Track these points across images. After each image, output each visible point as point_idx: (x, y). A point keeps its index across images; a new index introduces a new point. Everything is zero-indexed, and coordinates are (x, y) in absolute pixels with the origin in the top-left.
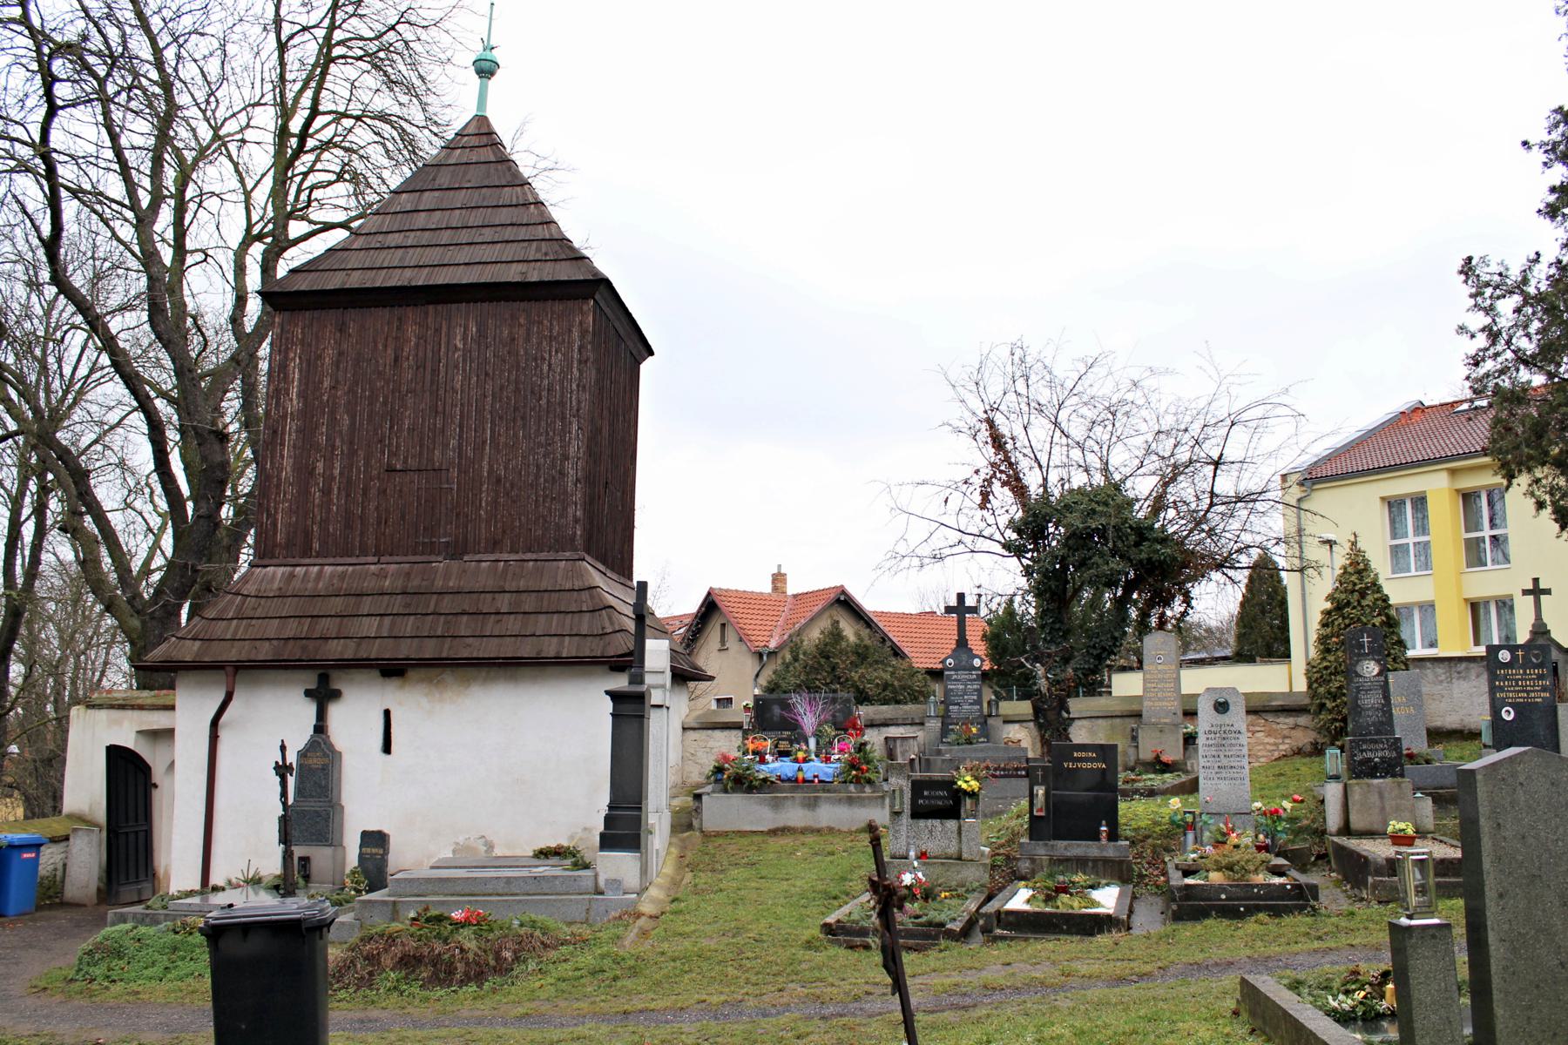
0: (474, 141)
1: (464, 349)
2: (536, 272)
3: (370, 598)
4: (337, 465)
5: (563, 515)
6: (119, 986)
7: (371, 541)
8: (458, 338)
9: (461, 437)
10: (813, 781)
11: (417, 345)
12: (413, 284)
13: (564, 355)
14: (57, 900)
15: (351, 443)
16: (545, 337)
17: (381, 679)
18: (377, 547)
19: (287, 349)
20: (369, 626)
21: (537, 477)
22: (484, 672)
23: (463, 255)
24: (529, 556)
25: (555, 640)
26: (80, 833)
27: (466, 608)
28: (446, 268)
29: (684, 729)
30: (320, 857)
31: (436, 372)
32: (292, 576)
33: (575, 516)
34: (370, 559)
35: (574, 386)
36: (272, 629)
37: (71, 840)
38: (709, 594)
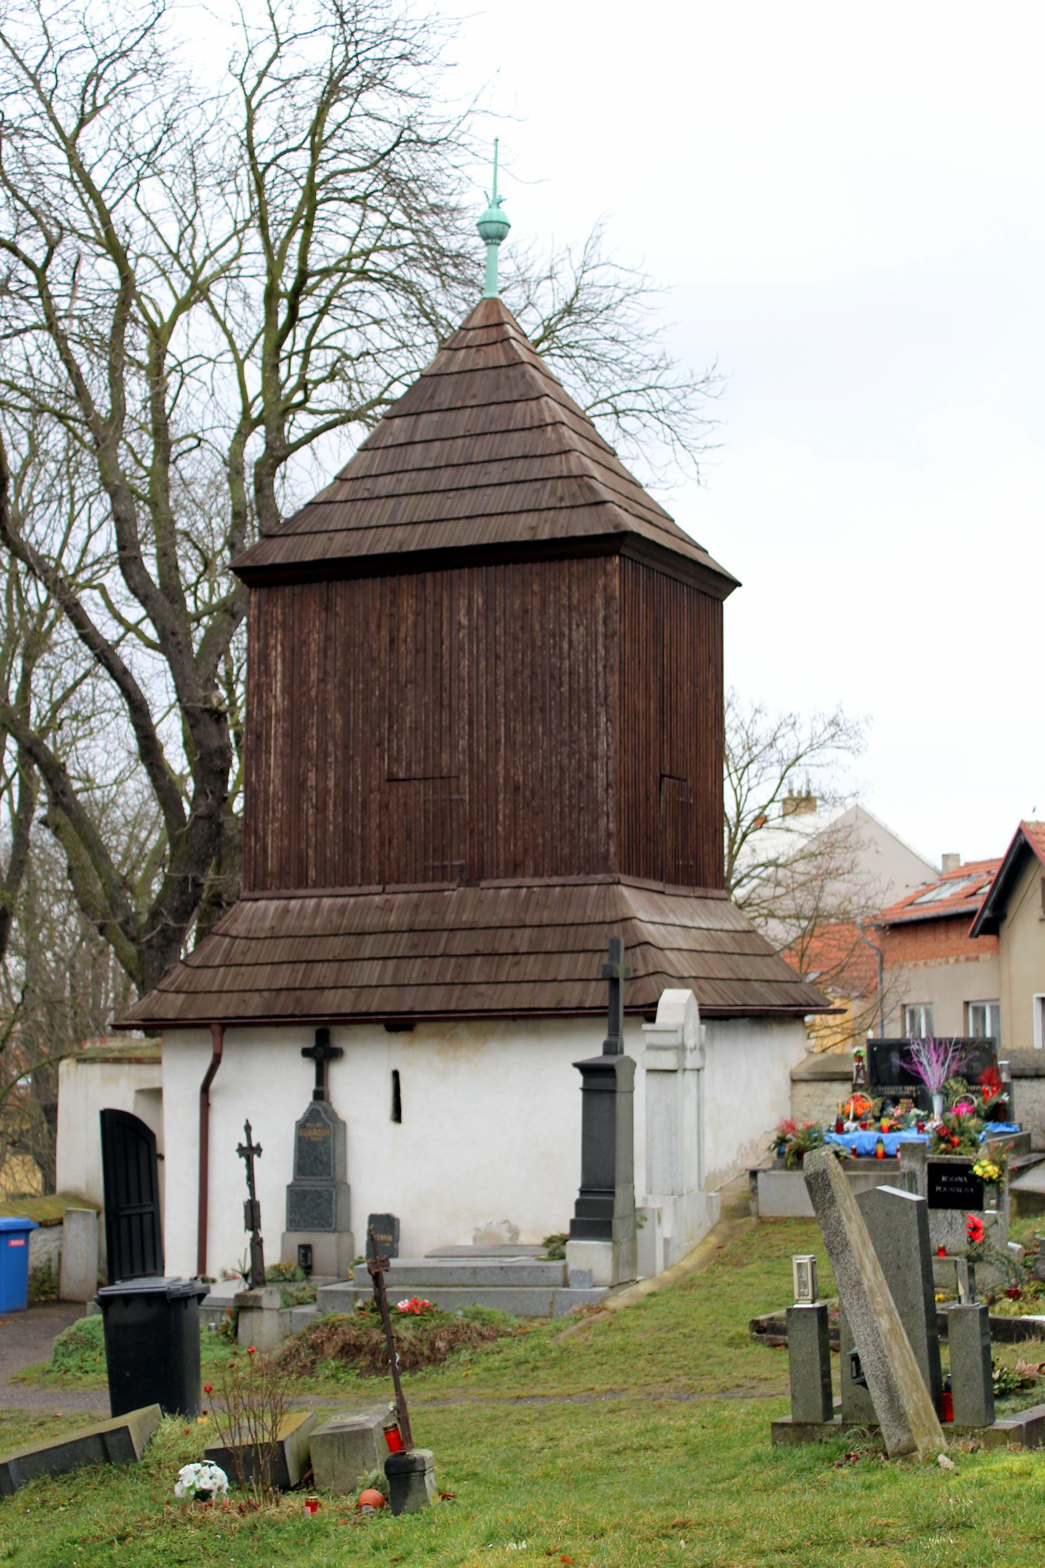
0: (481, 337)
1: (470, 626)
2: (548, 526)
3: (373, 937)
4: (331, 775)
5: (594, 827)
6: (92, 1375)
7: (374, 867)
8: (463, 612)
9: (471, 736)
10: (895, 1156)
11: (415, 624)
12: (405, 549)
13: (587, 629)
14: (53, 1297)
15: (346, 747)
16: (564, 607)
17: (387, 1034)
18: (381, 873)
19: (267, 636)
20: (370, 973)
21: (561, 783)
22: (502, 1025)
23: (465, 504)
24: (555, 880)
25: (578, 986)
26: (75, 1216)
27: (481, 947)
28: (443, 524)
29: (794, 1081)
30: (324, 1244)
31: (438, 656)
32: (286, 911)
33: (607, 829)
34: (376, 888)
35: (600, 668)
36: (262, 977)
37: (65, 1223)
38: (1020, 832)
